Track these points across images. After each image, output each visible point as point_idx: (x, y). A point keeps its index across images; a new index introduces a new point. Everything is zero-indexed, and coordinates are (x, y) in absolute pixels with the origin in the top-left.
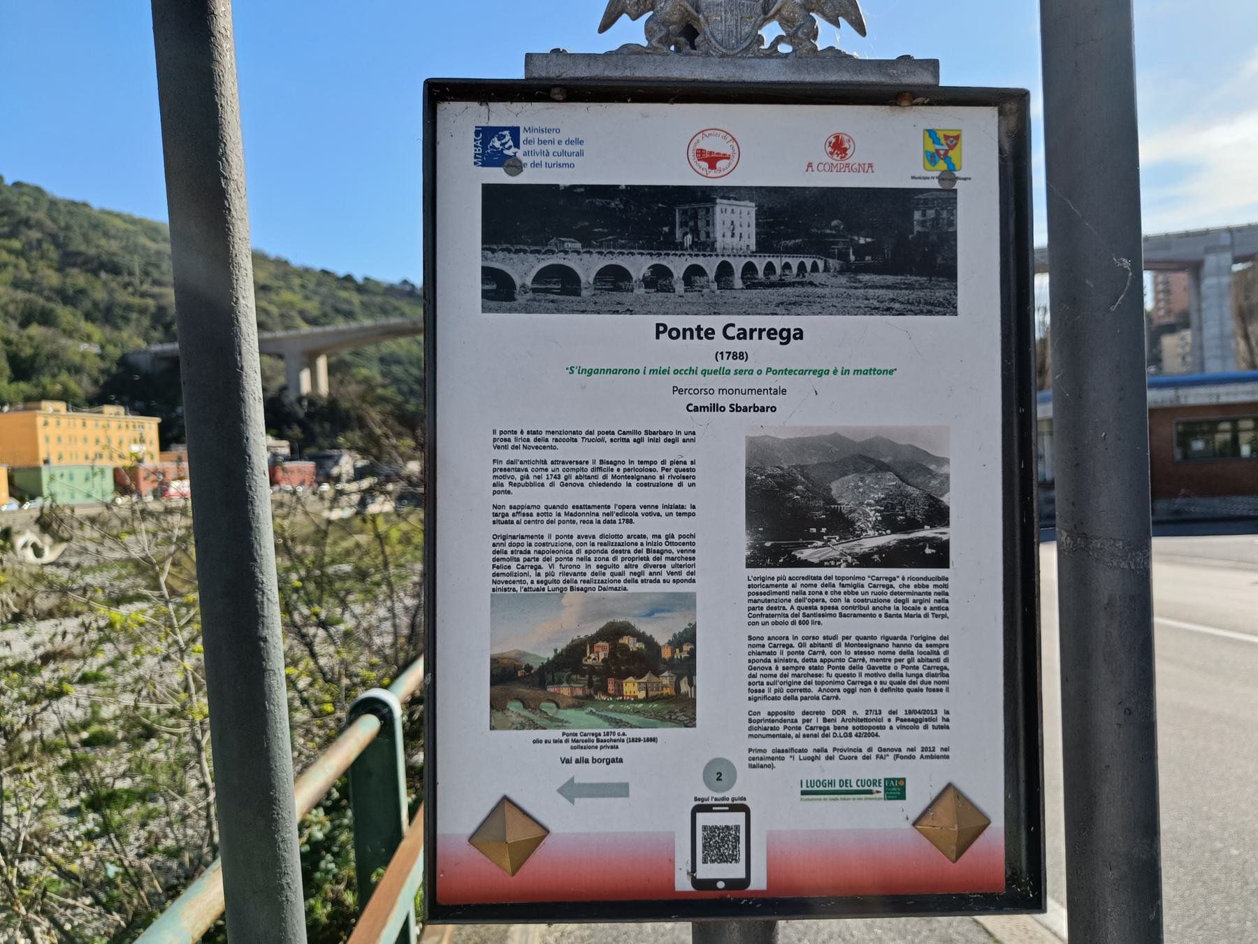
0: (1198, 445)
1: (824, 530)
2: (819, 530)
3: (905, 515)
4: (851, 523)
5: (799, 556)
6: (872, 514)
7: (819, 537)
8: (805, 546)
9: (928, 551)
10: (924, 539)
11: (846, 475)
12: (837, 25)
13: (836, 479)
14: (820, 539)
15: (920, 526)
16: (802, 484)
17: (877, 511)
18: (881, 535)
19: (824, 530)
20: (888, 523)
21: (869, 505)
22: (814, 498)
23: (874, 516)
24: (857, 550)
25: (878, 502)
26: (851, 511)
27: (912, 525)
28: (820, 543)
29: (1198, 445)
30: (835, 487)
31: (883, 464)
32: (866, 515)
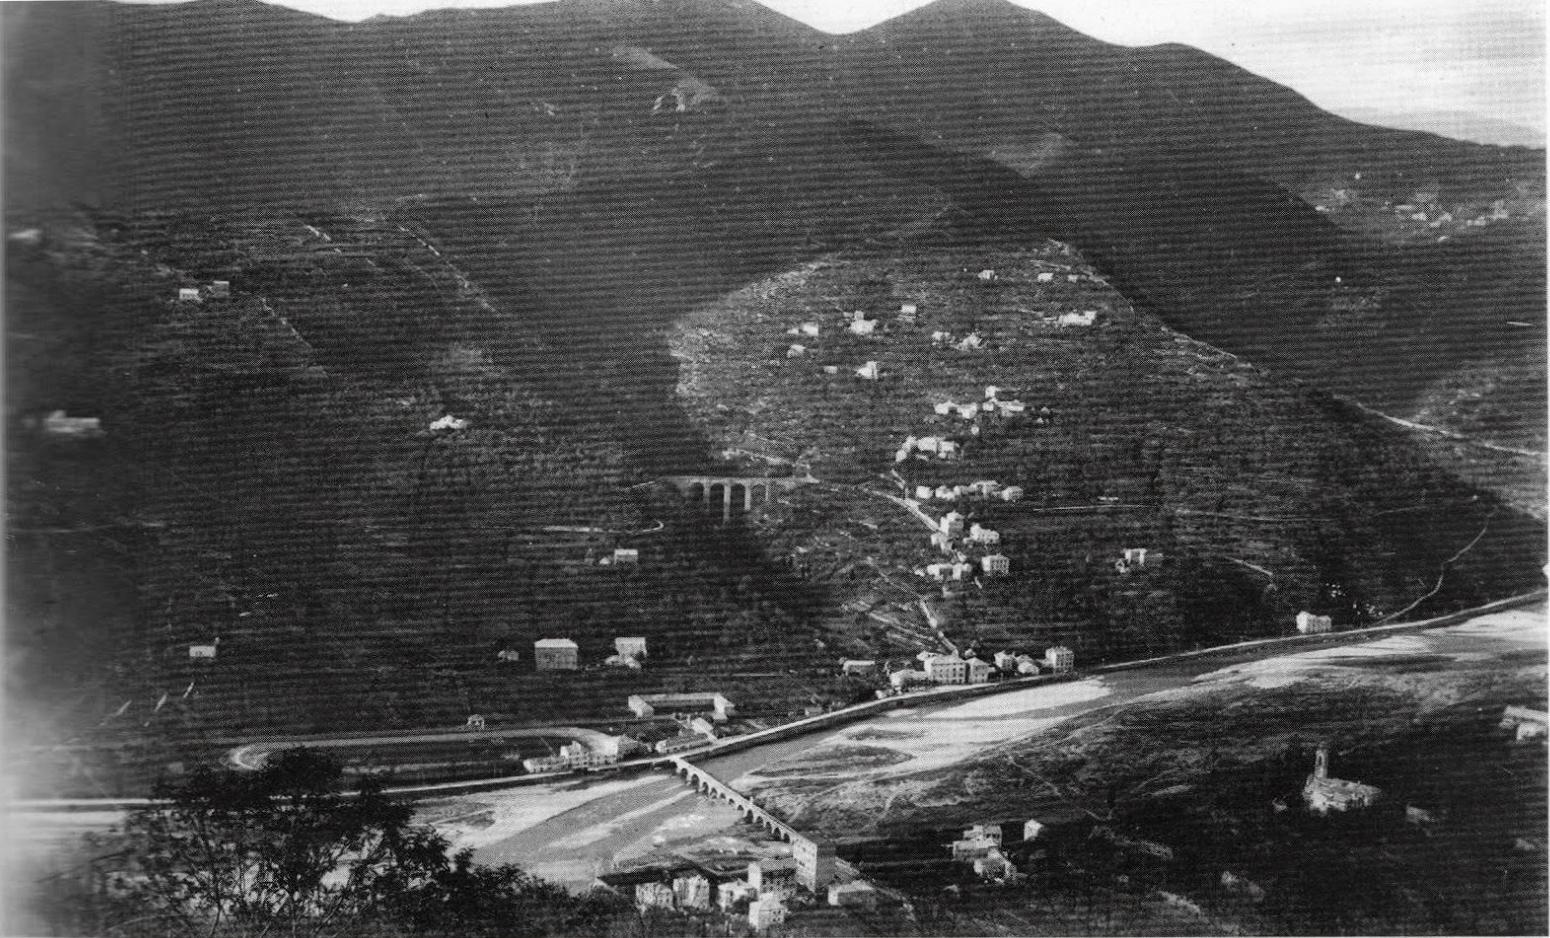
0: (605, 561)
1: (630, 649)
2: (594, 648)
3: (1160, 537)
4: (802, 602)
5: (461, 837)
6: (943, 529)
7: (593, 698)
8: (497, 768)
9: (1322, 794)
10: (1294, 708)
11: (764, 265)
12: (603, 878)
13: (697, 298)
14: (604, 713)
15: (1258, 618)
16: (482, 329)
17: (975, 510)
18: (1007, 681)
19: (630, 649)
20: (1047, 603)
21: (921, 469)
22: (560, 426)
23: (952, 541)
24: (853, 792)
25: (983, 448)
26: (809, 516)
27: (1225, 609)
28: (608, 746)
29: (605, 561)
30: (696, 348)
31: (1003, 181)
32: (909, 541)
